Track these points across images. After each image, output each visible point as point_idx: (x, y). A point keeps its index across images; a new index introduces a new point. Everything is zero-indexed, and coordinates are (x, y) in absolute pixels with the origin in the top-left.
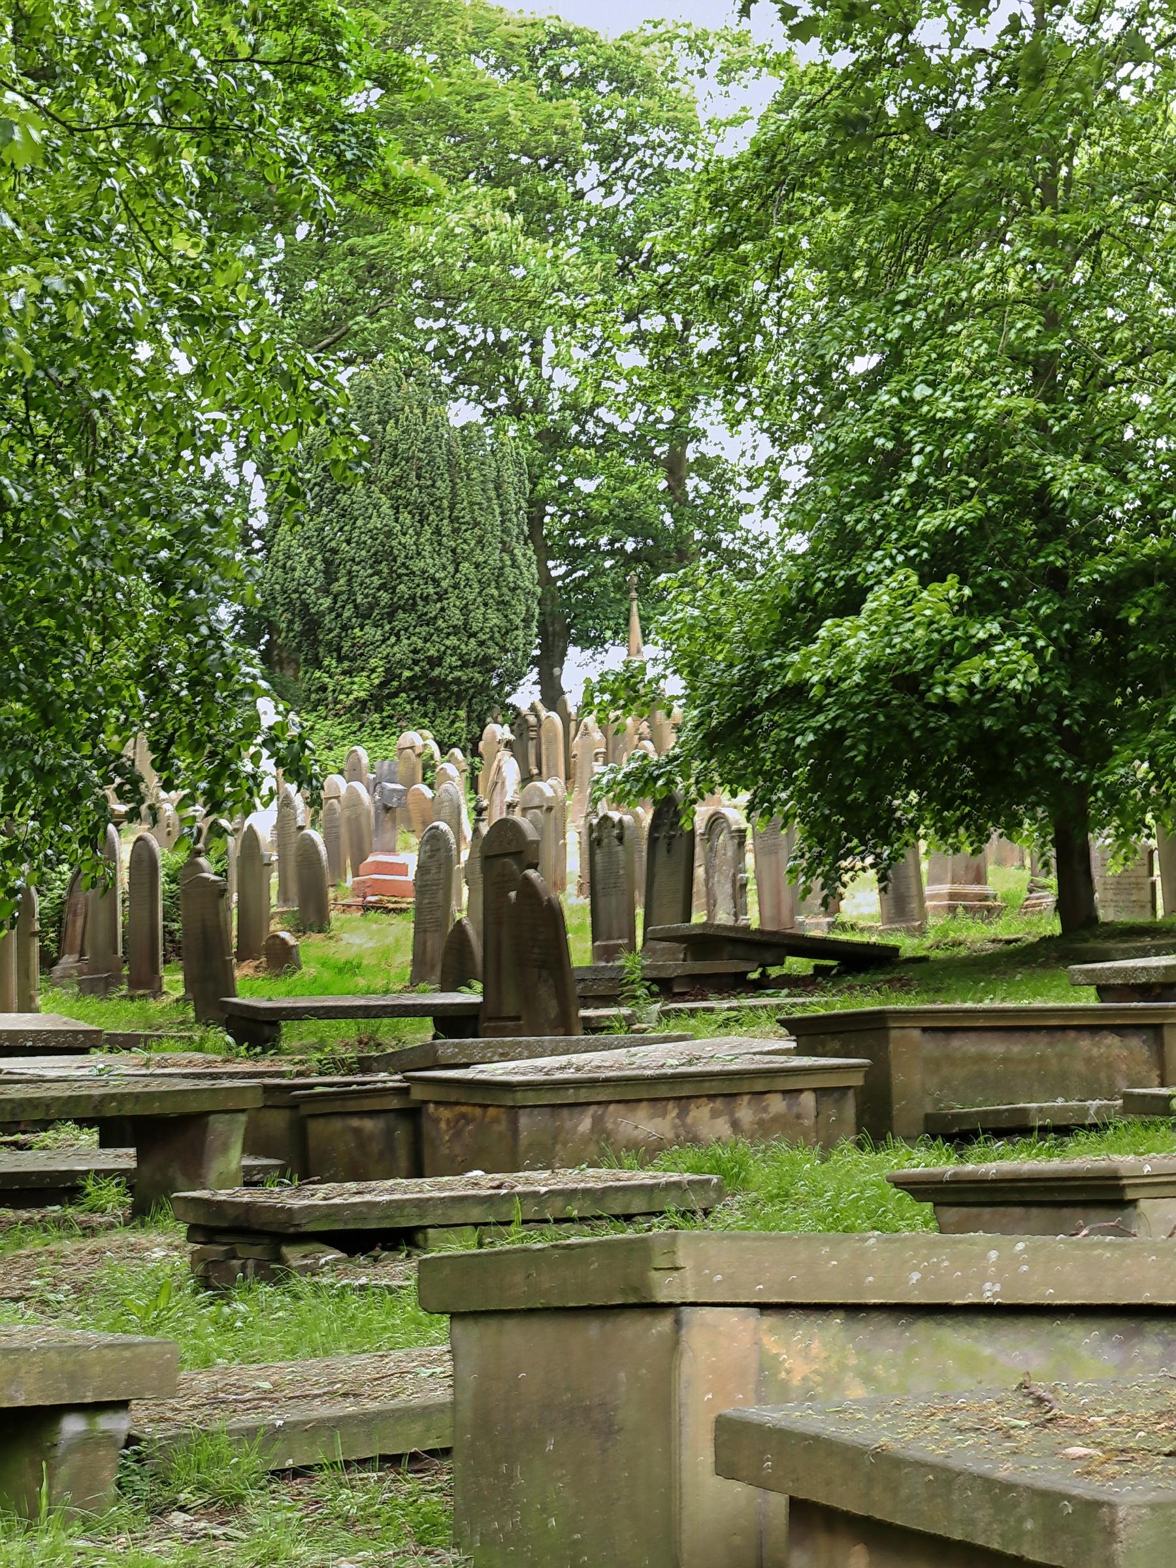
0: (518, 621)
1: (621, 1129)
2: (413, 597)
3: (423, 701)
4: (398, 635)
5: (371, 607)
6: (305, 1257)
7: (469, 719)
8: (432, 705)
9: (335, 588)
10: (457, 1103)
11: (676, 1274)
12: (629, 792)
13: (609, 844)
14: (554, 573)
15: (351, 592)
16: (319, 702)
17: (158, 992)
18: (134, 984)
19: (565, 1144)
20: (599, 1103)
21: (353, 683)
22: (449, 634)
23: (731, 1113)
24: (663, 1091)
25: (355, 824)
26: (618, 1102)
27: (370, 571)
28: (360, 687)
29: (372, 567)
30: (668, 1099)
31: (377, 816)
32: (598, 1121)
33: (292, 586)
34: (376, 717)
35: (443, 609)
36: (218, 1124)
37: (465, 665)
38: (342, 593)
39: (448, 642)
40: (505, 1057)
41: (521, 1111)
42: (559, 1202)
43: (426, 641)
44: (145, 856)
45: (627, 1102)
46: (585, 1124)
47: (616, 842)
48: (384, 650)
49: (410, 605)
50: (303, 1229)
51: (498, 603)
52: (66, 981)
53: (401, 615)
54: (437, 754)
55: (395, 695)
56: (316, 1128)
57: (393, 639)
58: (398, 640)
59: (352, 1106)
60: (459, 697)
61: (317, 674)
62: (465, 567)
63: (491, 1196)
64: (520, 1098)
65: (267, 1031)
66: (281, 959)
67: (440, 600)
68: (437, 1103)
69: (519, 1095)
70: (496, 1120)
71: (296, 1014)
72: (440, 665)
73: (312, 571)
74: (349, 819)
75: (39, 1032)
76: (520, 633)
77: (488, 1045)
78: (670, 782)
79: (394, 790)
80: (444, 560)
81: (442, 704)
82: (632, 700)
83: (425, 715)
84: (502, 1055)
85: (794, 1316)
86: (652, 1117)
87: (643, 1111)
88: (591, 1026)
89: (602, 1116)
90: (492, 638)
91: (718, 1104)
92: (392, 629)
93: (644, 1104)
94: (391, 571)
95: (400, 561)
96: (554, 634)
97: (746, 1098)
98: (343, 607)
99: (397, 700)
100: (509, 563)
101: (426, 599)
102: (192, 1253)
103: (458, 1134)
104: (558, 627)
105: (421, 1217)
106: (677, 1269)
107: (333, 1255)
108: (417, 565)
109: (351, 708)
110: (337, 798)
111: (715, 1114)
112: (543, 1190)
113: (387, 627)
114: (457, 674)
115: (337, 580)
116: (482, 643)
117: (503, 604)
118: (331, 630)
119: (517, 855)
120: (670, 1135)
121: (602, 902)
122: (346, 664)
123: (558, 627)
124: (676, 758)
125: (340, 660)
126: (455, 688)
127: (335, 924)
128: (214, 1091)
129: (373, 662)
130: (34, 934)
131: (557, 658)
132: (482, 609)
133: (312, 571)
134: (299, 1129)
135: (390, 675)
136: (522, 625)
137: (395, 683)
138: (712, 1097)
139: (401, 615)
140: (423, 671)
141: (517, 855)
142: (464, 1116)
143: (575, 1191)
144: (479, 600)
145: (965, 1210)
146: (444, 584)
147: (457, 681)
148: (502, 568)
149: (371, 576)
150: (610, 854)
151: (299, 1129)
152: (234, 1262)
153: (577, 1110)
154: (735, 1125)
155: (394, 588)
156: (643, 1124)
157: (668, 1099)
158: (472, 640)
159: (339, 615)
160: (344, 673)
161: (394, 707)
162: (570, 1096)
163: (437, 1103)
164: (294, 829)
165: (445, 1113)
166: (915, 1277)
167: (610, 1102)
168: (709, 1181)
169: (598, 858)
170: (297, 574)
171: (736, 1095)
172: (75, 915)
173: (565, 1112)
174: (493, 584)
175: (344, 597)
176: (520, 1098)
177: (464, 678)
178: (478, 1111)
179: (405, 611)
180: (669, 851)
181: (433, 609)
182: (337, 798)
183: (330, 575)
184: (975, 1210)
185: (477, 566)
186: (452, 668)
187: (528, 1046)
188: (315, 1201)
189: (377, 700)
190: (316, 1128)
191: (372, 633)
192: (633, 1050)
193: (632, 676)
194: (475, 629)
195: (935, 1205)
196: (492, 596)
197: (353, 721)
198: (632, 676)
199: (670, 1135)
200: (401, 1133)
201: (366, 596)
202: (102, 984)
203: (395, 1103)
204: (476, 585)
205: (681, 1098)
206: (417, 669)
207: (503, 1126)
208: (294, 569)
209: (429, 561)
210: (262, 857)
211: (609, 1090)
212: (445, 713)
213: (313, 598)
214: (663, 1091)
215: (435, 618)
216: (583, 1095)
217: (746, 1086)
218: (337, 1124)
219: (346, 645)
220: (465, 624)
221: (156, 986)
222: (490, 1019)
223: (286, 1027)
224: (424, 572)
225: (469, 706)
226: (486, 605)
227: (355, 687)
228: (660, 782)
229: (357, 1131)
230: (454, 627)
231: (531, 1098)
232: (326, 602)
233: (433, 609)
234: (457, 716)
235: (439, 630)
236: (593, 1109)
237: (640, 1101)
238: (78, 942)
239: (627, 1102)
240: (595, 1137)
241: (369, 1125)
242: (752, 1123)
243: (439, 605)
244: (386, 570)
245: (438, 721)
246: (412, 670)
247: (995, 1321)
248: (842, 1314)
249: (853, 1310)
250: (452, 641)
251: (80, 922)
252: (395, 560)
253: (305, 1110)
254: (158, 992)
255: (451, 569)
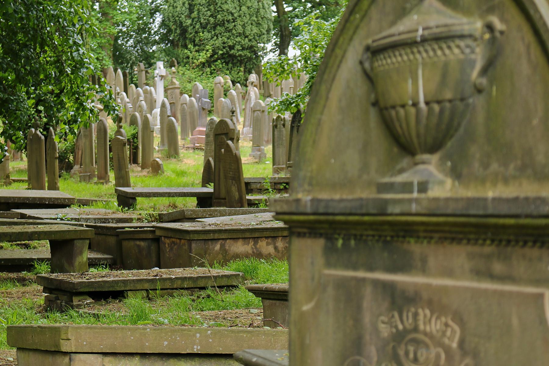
0: (264, 32)
1: (232, 249)
2: (223, 20)
3: (227, 64)
4: (217, 36)
5: (207, 24)
6: (79, 301)
7: (245, 72)
8: (230, 65)
9: (193, 15)
10: (171, 237)
11: (68, 341)
12: (282, 109)
13: (280, 127)
14: (286, 10)
15: (199, 18)
16: (187, 63)
17: (108, 181)
18: (100, 178)
19: (209, 255)
20: (223, 239)
21: (200, 55)
22: (237, 36)
23: (275, 244)
24: (248, 235)
25: (192, 114)
26: (230, 239)
27: (206, 9)
28: (203, 57)
29: (207, 7)
30: (250, 238)
31: (200, 112)
32: (222, 246)
33: (176, 14)
34: (208, 69)
35: (235, 26)
36: (78, 243)
37: (243, 49)
38: (195, 18)
39: (236, 40)
40: (211, 216)
41: (192, 242)
42: (179, 282)
43: (228, 39)
44: (102, 127)
45: (234, 239)
46: (218, 247)
47: (282, 126)
48: (212, 42)
49: (222, 24)
50: (78, 291)
51: (257, 23)
52: (75, 176)
53: (218, 28)
54: (231, 85)
55: (216, 61)
56: (125, 244)
57: (215, 38)
58: (217, 38)
59: (137, 236)
60: (241, 62)
61: (186, 51)
62: (244, 8)
63: (152, 280)
64: (192, 236)
65: (131, 201)
66: (156, 169)
67: (234, 22)
68: (165, 237)
69: (191, 236)
70: (184, 245)
71: (142, 195)
72: (233, 49)
73: (184, 8)
74: (190, 113)
75: (50, 198)
76: (265, 36)
77: (204, 211)
78: (297, 106)
79: (206, 102)
80: (236, 5)
81: (234, 65)
82: (283, 72)
83: (228, 69)
84: (210, 215)
85: (119, 357)
86: (244, 245)
87: (240, 242)
88: (251, 204)
89: (224, 244)
90: (254, 38)
91: (270, 240)
92: (215, 33)
93: (241, 240)
94: (215, 9)
95: (219, 5)
96: (286, 35)
97: (280, 238)
98: (196, 24)
99: (217, 63)
100: (261, 7)
101: (228, 21)
102: (46, 297)
103: (171, 249)
104: (287, 33)
105: (125, 287)
106: (69, 340)
107: (89, 300)
108: (225, 7)
109: (198, 66)
110: (186, 104)
111: (268, 244)
112: (174, 277)
113: (213, 33)
114: (240, 53)
115: (193, 12)
116: (250, 40)
117: (258, 24)
118: (191, 33)
119: (226, 134)
120: (250, 252)
121: (276, 150)
122: (197, 48)
123: (287, 33)
124: (299, 95)
125: (195, 45)
126: (239, 58)
127: (181, 155)
128: (76, 231)
129: (208, 47)
130: (56, 158)
131: (286, 46)
132: (251, 26)
133: (184, 8)
134: (119, 244)
135: (214, 53)
136: (266, 33)
137: (216, 56)
138: (267, 238)
139: (218, 28)
140: (227, 51)
141: (226, 134)
142: (173, 242)
143: (186, 278)
144: (249, 22)
145: (271, 301)
146: (236, 15)
147: (240, 56)
148: (258, 9)
149: (207, 11)
150: (280, 131)
151: (119, 244)
152: (58, 301)
153: (215, 241)
154: (276, 248)
155: (216, 17)
156: (239, 247)
157: (250, 238)
158: (246, 39)
159: (194, 27)
160: (196, 51)
161: (215, 66)
162: (211, 236)
163: (165, 237)
164: (166, 117)
165: (167, 241)
166: (166, 343)
167: (227, 239)
168: (239, 274)
169: (276, 133)
170: (178, 9)
171: (276, 237)
172: (79, 149)
173: (210, 242)
174: (255, 15)
175: (196, 20)
176: (192, 236)
177: (243, 54)
178: (178, 241)
179: (220, 26)
180: (298, 132)
181: (231, 26)
182: (186, 104)
183: (191, 11)
184: (274, 302)
185: (248, 8)
186: (238, 50)
187: (220, 211)
188: (84, 280)
189: (209, 63)
190: (125, 244)
191: (207, 35)
192: (256, 214)
193: (282, 63)
194: (247, 34)
195: (18, 349)
196: (254, 21)
197: (200, 71)
198: (282, 63)
199: (250, 252)
200: (153, 247)
201: (205, 19)
202: (88, 178)
203: (150, 236)
204: (248, 16)
205: (254, 238)
206: (224, 50)
207: (186, 247)
208: (177, 7)
209: (230, 5)
210: (150, 128)
211: (227, 234)
212: (235, 69)
213: (184, 19)
214: (248, 235)
215: (232, 29)
216: (216, 236)
217: (280, 234)
218: (132, 243)
219: (197, 40)
220: (244, 32)
221: (107, 179)
222: (216, 199)
223: (139, 199)
224: (228, 10)
225: (245, 66)
226: (252, 24)
227: (200, 57)
228: (293, 105)
229: (139, 246)
230: (240, 33)
231: (196, 237)
232: (189, 22)
233: (231, 26)
234: (240, 70)
235: (233, 34)
236: (220, 241)
237: (239, 238)
238: (80, 160)
239: (234, 239)
240: (221, 252)
241: (142, 244)
242: (282, 248)
243: (233, 24)
244: (213, 9)
245: (233, 72)
246: (222, 50)
247: (201, 360)
248: (139, 357)
249: (143, 355)
250: (238, 39)
251: (80, 153)
252: (216, 4)
253: (121, 237)
254: (108, 181)
255: (238, 8)
